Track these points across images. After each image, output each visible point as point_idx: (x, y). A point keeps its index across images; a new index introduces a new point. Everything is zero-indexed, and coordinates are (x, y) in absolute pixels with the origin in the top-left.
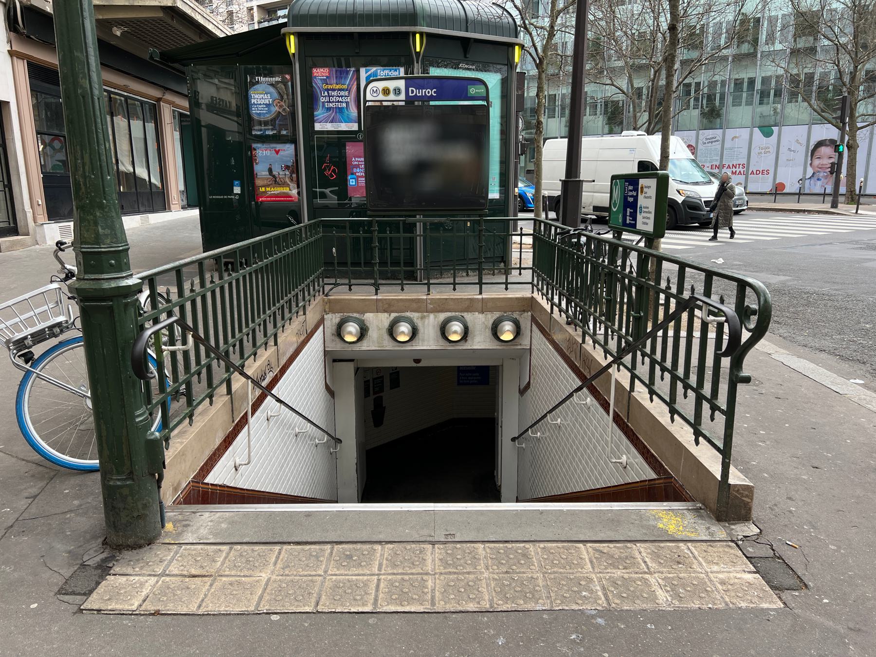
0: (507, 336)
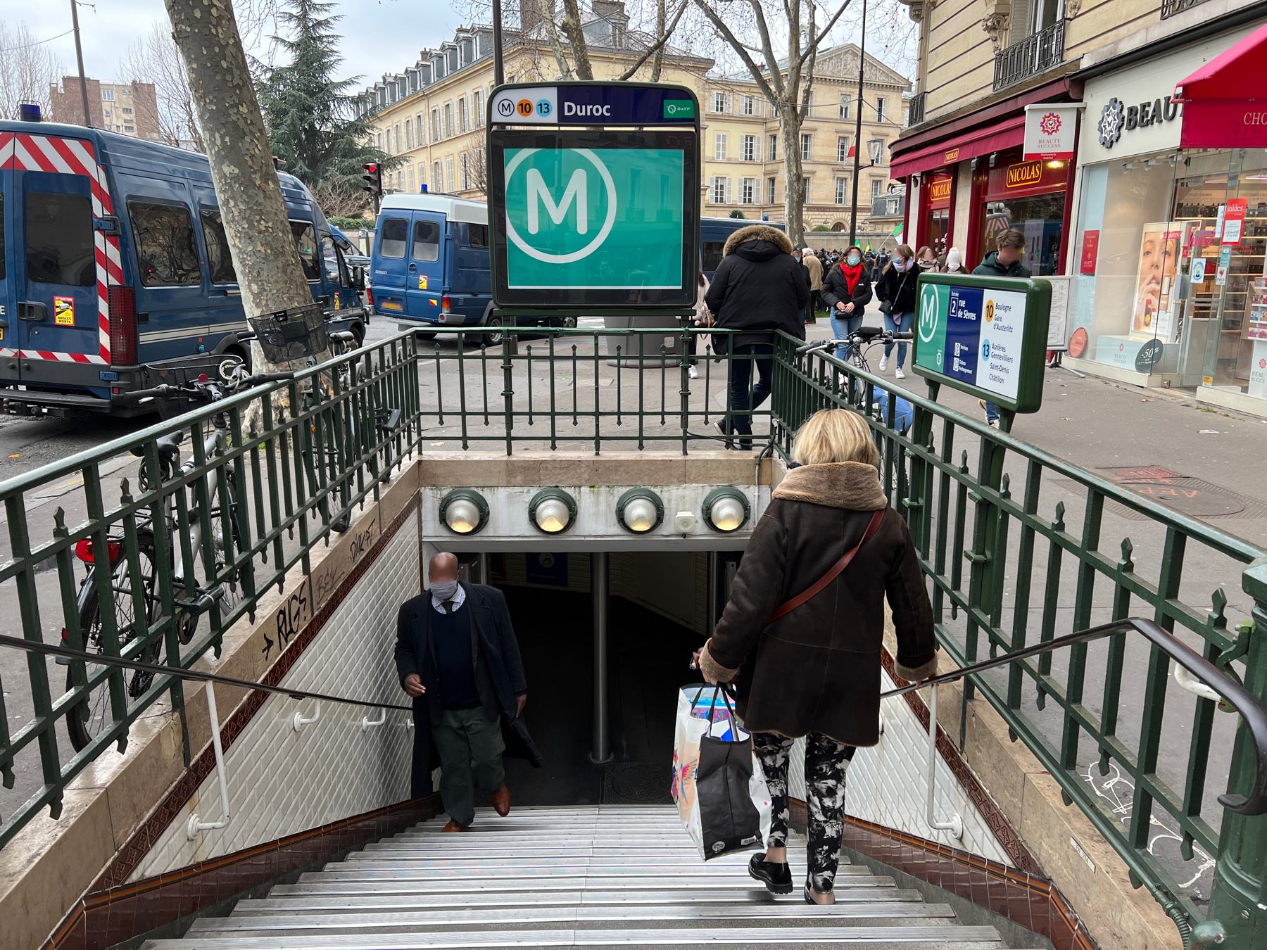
0: (553, 525)
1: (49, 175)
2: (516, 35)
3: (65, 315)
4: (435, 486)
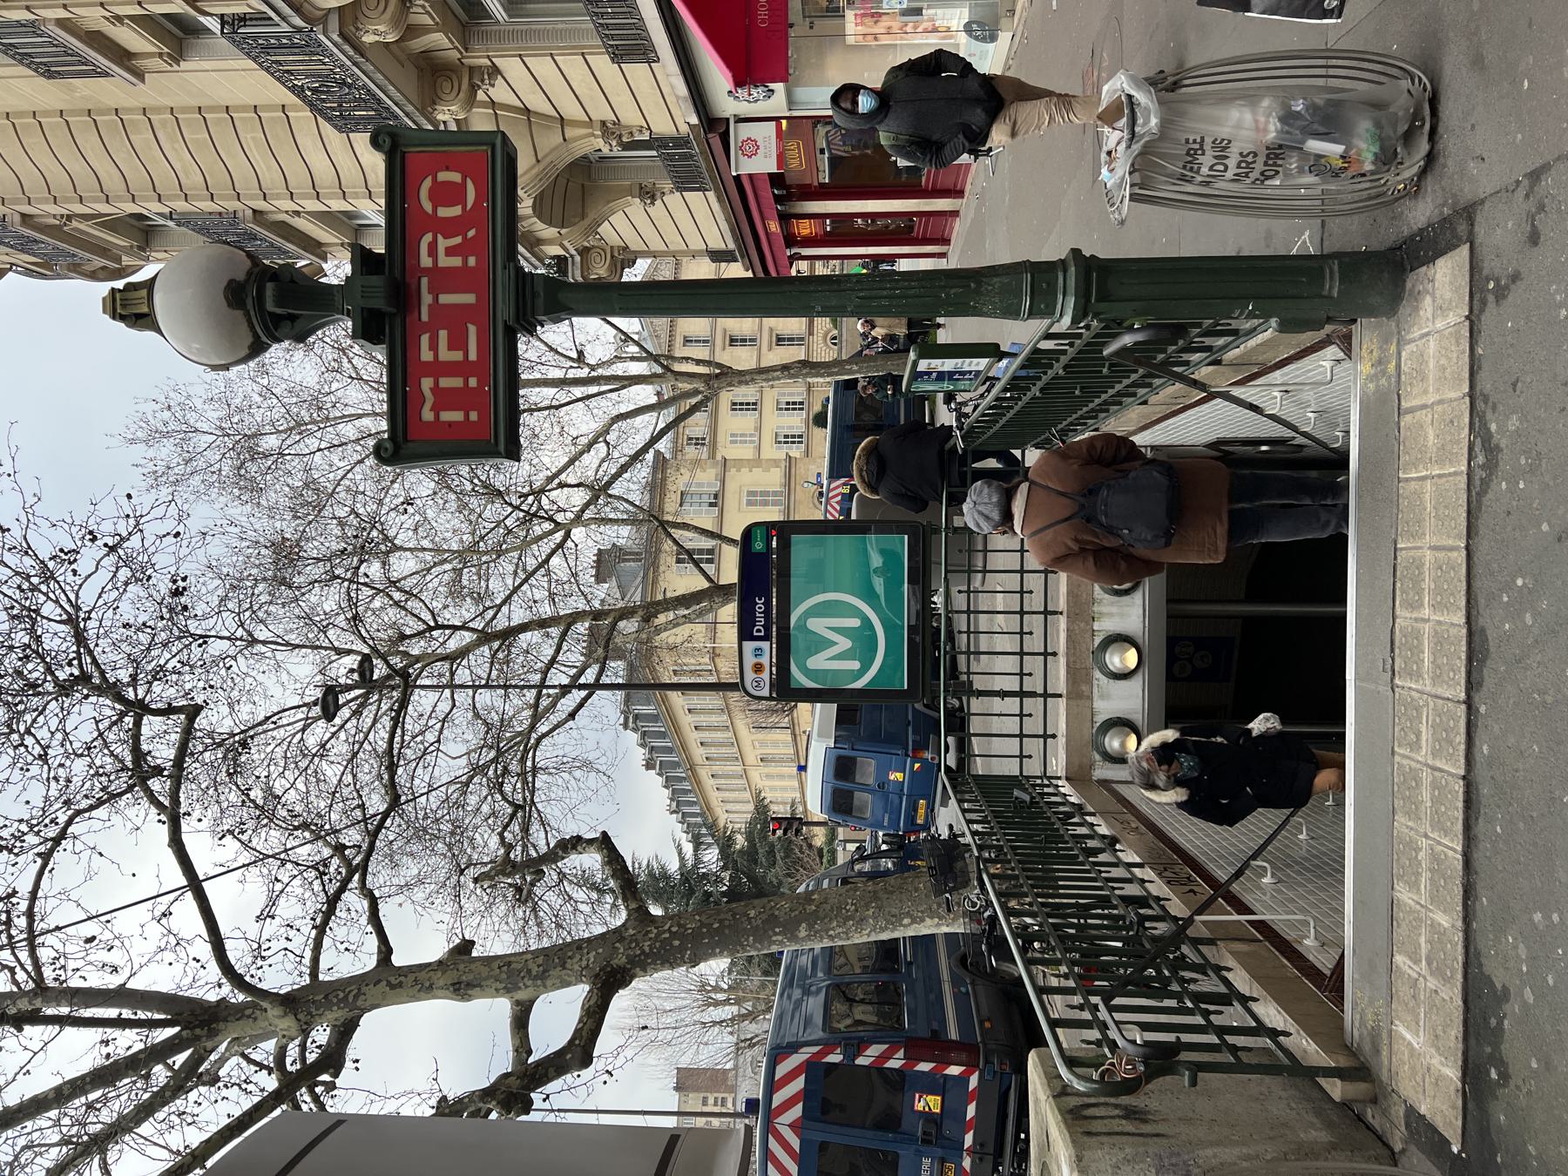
0: (1131, 658)
1: (806, 1095)
2: (631, 668)
3: (931, 1103)
4: (1091, 766)
